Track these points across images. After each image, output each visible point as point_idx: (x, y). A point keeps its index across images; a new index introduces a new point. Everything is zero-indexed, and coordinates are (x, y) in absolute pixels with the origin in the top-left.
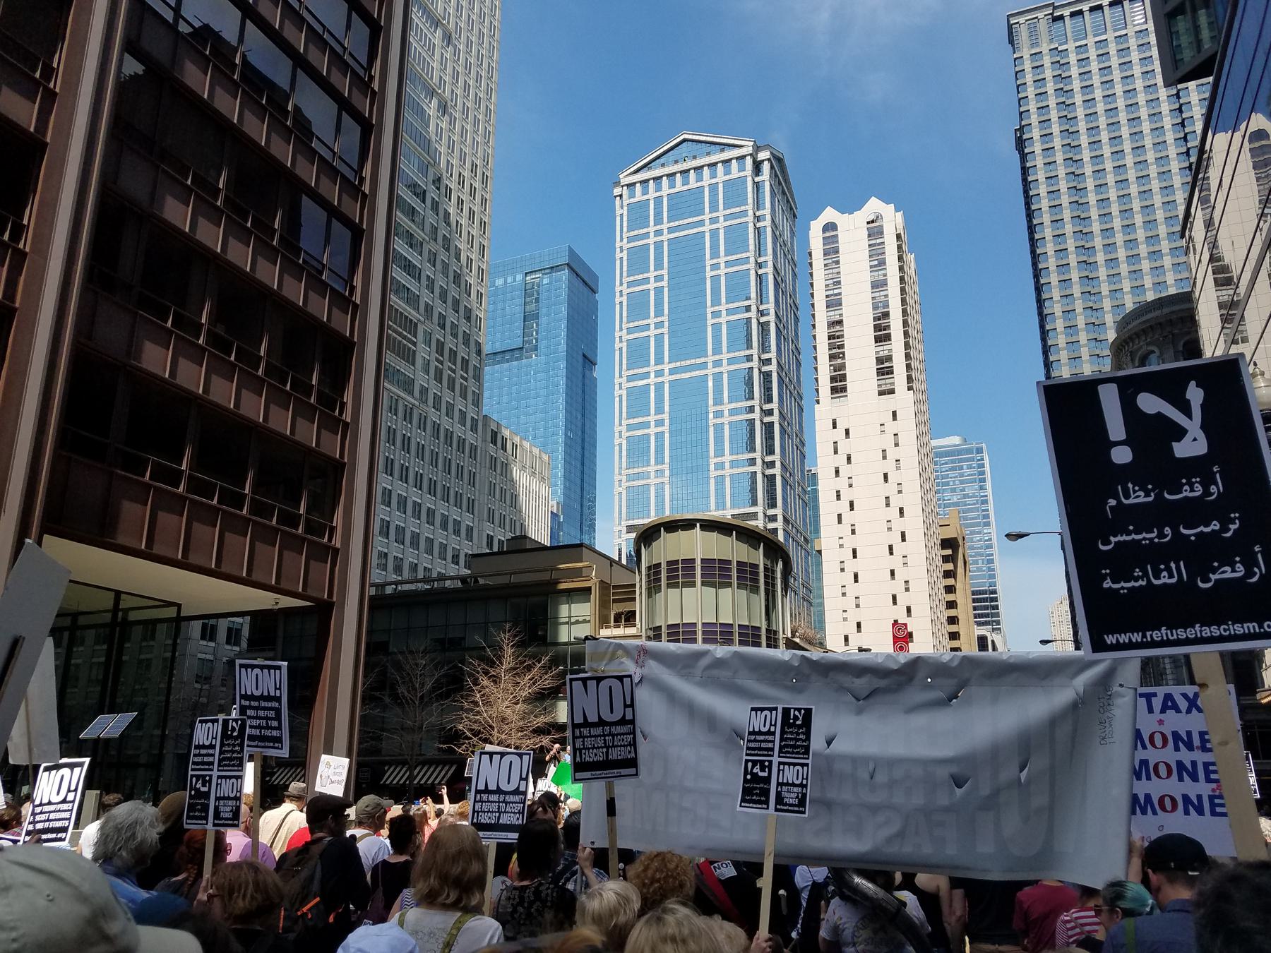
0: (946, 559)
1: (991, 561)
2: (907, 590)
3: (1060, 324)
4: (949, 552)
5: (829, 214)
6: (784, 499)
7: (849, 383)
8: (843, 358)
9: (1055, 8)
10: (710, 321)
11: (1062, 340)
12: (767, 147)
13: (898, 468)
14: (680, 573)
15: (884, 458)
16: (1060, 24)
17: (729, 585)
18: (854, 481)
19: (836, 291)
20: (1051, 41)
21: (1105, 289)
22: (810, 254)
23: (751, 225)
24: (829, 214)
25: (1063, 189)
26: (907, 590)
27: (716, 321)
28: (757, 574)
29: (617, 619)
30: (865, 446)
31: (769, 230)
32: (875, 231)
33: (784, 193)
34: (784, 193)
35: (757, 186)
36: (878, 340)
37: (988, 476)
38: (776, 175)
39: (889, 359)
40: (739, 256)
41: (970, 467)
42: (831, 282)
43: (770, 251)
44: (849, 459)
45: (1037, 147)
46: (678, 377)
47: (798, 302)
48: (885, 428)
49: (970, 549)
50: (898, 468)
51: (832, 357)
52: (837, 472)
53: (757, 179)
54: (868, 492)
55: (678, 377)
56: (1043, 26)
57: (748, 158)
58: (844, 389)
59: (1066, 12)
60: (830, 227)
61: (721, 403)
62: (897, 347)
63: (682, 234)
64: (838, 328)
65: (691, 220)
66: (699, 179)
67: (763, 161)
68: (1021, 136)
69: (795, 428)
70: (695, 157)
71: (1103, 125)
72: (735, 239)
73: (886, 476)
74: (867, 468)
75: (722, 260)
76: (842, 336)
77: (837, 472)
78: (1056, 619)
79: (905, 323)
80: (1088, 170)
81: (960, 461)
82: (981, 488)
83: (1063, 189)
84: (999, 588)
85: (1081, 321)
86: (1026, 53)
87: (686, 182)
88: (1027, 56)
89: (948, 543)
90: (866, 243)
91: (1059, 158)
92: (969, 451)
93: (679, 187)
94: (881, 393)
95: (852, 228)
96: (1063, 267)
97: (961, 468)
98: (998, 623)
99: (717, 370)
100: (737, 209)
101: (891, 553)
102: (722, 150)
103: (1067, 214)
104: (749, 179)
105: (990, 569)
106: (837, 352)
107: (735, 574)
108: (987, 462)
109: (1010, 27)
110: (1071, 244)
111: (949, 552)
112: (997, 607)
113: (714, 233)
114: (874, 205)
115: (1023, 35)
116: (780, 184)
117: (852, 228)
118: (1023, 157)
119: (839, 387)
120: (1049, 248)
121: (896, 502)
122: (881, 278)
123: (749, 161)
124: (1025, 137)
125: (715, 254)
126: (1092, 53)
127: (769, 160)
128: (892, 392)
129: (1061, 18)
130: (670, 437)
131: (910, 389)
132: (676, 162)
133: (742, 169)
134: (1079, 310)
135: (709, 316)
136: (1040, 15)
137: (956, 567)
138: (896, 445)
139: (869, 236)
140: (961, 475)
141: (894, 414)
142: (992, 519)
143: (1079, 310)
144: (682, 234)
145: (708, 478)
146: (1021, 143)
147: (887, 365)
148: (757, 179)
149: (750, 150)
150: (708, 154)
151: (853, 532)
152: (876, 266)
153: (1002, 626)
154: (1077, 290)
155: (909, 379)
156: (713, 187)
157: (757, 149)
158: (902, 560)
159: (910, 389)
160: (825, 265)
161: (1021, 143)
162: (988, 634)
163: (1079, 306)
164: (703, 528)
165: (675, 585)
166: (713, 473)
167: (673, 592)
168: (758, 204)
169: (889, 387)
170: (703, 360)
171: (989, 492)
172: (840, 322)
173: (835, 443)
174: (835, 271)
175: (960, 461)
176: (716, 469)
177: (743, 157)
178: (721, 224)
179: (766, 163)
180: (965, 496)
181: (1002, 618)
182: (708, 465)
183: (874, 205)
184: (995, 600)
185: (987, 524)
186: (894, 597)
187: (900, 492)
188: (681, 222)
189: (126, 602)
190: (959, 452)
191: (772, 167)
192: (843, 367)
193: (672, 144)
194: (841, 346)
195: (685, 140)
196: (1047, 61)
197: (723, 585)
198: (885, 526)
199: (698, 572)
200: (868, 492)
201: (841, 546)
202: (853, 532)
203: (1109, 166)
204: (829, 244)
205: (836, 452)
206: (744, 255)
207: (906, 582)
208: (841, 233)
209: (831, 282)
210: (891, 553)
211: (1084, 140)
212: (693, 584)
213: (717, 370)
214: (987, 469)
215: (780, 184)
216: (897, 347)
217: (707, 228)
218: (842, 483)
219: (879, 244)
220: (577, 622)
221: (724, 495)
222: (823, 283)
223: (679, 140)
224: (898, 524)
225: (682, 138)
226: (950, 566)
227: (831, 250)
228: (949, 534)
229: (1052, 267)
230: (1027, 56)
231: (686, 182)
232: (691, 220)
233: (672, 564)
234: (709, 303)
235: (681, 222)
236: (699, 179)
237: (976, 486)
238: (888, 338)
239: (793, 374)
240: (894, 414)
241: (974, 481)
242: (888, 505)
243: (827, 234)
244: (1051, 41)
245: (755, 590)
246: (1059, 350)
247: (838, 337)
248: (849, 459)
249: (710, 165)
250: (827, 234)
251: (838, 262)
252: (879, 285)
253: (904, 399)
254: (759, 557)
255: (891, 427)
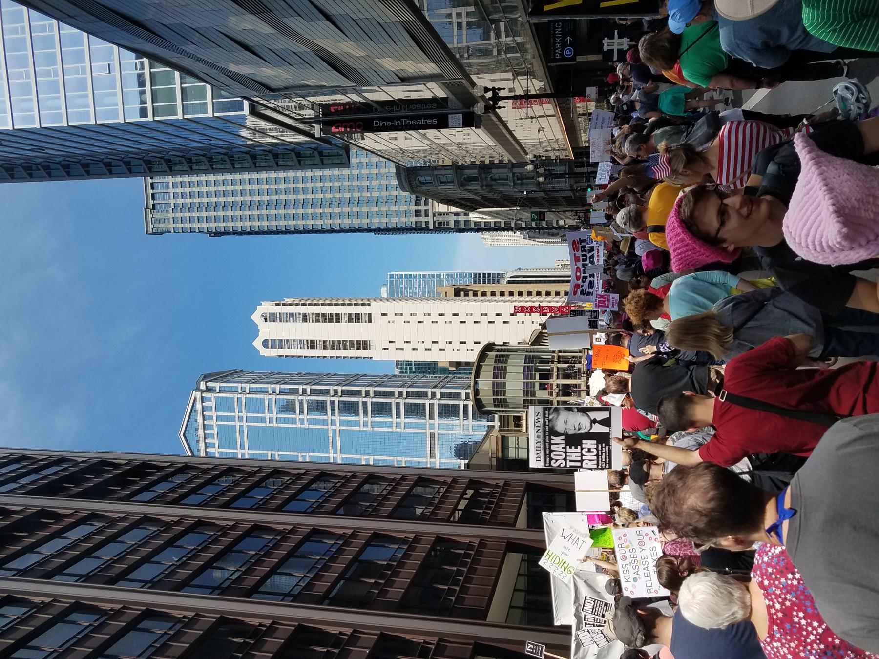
0: (466, 295)
1: (461, 275)
2: (486, 315)
3: (337, 221)
4: (462, 293)
5: (258, 344)
6: (422, 387)
7: (362, 339)
8: (346, 341)
9: (147, 208)
10: (306, 426)
11: (329, 222)
12: (198, 383)
13: (416, 315)
14: (499, 390)
15: (409, 322)
16: (158, 207)
17: (505, 367)
18: (421, 340)
19: (305, 343)
20: (167, 212)
21: (320, 196)
22: (280, 356)
23: (247, 396)
24: (258, 344)
25: (206, 214)
26: (486, 315)
27: (306, 422)
28: (500, 355)
29: (517, 425)
30: (400, 333)
31: (251, 385)
32: (271, 318)
33: (227, 376)
34: (227, 376)
35: (222, 391)
36: (338, 321)
37: (408, 273)
38: (216, 379)
39: (350, 315)
40: (266, 405)
41: (401, 283)
42: (299, 345)
43: (265, 386)
44: (407, 342)
45: (222, 224)
46: (339, 448)
47: (297, 373)
48: (391, 320)
49: (461, 283)
50: (416, 315)
51: (345, 348)
52: (414, 349)
53: (218, 391)
54: (427, 333)
55: (339, 448)
56: (157, 215)
57: (203, 395)
58: (365, 342)
59: (152, 202)
60: (265, 344)
61: (359, 422)
62: (343, 310)
63: (246, 441)
64: (328, 343)
65: (238, 434)
66: (212, 427)
67: (206, 386)
68: (214, 233)
69: (377, 379)
70: (197, 429)
71: (232, 188)
72: (255, 406)
73: (419, 322)
74: (414, 333)
75: (267, 415)
76: (333, 341)
77: (414, 349)
78: (495, 243)
79: (330, 305)
80: (248, 198)
81: (397, 288)
82: (415, 277)
83: (206, 214)
84: (473, 272)
85: (337, 210)
86: (172, 226)
87: (212, 436)
88: (174, 226)
89: (457, 292)
90: (278, 323)
91: (239, 213)
92: (391, 282)
93: (215, 441)
94: (370, 321)
95: (268, 331)
96: (216, 219)
97: (402, 288)
98: (498, 274)
99: (337, 423)
100: (236, 404)
101: (465, 322)
102: (195, 411)
103: (273, 212)
104: (217, 395)
105: (466, 276)
106: (343, 345)
107: (500, 364)
108: (399, 273)
109: (154, 233)
110: (195, 214)
111: (462, 293)
112: (489, 275)
113: (249, 419)
114: (256, 317)
115: (161, 226)
116: (221, 377)
117: (268, 331)
118: (226, 233)
119: (363, 345)
120: (265, 224)
121: (435, 317)
122: (301, 316)
123: (205, 395)
124: (214, 231)
125: (263, 420)
126: (179, 190)
127: (206, 382)
128: (370, 315)
129: (154, 205)
130: (377, 455)
131: (369, 305)
132: (198, 441)
133: (210, 399)
134: (330, 210)
135: (302, 426)
136: (150, 216)
137: (471, 290)
138: (402, 315)
139: (274, 321)
140: (406, 288)
141: (383, 315)
142: (436, 273)
143: (330, 210)
144: (246, 441)
145: (405, 433)
146: (218, 234)
147: (353, 317)
148: (218, 391)
149: (198, 394)
150: (196, 420)
151: (450, 342)
152: (293, 319)
153: (500, 272)
154: (319, 211)
155: (363, 305)
156: (219, 418)
157: (198, 389)
158: (469, 317)
159: (369, 305)
160: (288, 348)
161: (218, 234)
162: (506, 280)
163: (328, 210)
164: (478, 377)
165: (505, 391)
166: (403, 430)
167: (521, 369)
168: (234, 391)
169: (367, 317)
170: (330, 432)
171: (419, 273)
172: (324, 342)
173: (397, 349)
174: (293, 342)
175: (397, 288)
176: (400, 427)
177: (202, 398)
178: (244, 414)
179: (208, 384)
180: (419, 287)
181: (496, 271)
182: (397, 432)
183: (256, 317)
184: (484, 275)
185: (438, 276)
186: (490, 322)
187: (429, 315)
188: (238, 440)
189: (522, 572)
190: (392, 289)
191: (211, 381)
192: (351, 342)
193: (185, 444)
194: (339, 342)
195: (184, 435)
196: (179, 215)
197: (505, 370)
198: (448, 324)
199: (499, 380)
200: (427, 333)
201: (458, 350)
202: (450, 342)
203: (248, 187)
204: (275, 345)
205: (402, 349)
206: (266, 402)
207: (482, 315)
208: (270, 337)
209: (299, 345)
210: (465, 322)
211: (231, 199)
212: (505, 383)
213: (337, 423)
214: (403, 273)
215: (221, 377)
216: (343, 310)
217: (245, 424)
218: (422, 347)
219: (280, 316)
220: (518, 444)
221: (417, 424)
222: (299, 350)
223: (183, 439)
224: (448, 317)
225: (182, 437)
226: (471, 293)
227: (280, 344)
228: (451, 292)
229: (233, 224)
230: (174, 226)
231: (212, 436)
232: (238, 434)
233: (495, 393)
234: (294, 426)
235: (238, 440)
236: (212, 427)
237: (414, 280)
238: (337, 315)
239: (343, 378)
240: (383, 315)
241: (410, 281)
242: (436, 322)
243: (270, 346)
244: (167, 212)
245: (508, 356)
246: (371, 222)
247: (333, 343)
248: (407, 342)
249: (204, 420)
250: (270, 346)
251: (288, 341)
252: (305, 318)
253: (375, 309)
254: (492, 354)
255: (391, 317)
